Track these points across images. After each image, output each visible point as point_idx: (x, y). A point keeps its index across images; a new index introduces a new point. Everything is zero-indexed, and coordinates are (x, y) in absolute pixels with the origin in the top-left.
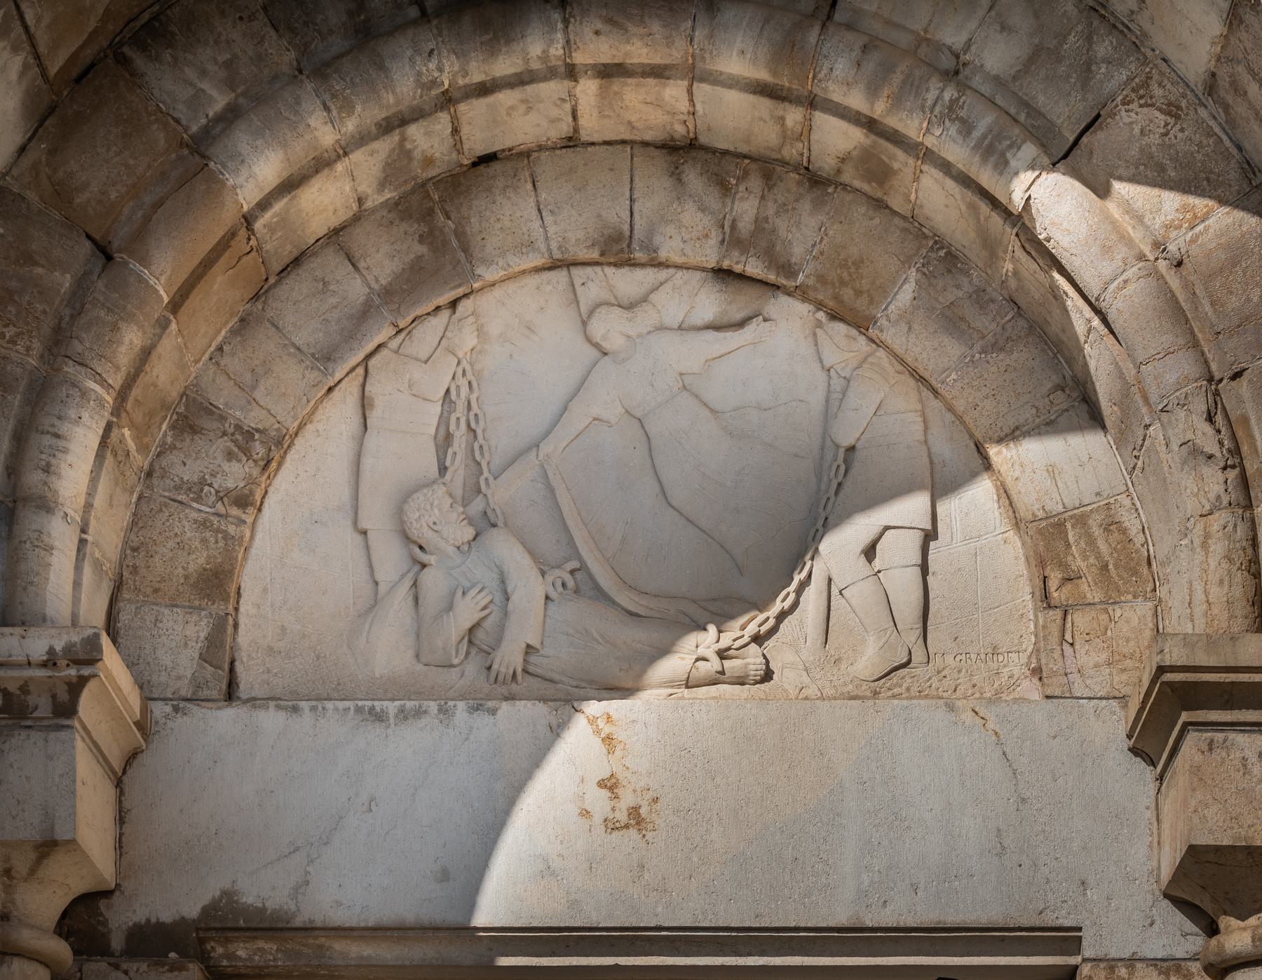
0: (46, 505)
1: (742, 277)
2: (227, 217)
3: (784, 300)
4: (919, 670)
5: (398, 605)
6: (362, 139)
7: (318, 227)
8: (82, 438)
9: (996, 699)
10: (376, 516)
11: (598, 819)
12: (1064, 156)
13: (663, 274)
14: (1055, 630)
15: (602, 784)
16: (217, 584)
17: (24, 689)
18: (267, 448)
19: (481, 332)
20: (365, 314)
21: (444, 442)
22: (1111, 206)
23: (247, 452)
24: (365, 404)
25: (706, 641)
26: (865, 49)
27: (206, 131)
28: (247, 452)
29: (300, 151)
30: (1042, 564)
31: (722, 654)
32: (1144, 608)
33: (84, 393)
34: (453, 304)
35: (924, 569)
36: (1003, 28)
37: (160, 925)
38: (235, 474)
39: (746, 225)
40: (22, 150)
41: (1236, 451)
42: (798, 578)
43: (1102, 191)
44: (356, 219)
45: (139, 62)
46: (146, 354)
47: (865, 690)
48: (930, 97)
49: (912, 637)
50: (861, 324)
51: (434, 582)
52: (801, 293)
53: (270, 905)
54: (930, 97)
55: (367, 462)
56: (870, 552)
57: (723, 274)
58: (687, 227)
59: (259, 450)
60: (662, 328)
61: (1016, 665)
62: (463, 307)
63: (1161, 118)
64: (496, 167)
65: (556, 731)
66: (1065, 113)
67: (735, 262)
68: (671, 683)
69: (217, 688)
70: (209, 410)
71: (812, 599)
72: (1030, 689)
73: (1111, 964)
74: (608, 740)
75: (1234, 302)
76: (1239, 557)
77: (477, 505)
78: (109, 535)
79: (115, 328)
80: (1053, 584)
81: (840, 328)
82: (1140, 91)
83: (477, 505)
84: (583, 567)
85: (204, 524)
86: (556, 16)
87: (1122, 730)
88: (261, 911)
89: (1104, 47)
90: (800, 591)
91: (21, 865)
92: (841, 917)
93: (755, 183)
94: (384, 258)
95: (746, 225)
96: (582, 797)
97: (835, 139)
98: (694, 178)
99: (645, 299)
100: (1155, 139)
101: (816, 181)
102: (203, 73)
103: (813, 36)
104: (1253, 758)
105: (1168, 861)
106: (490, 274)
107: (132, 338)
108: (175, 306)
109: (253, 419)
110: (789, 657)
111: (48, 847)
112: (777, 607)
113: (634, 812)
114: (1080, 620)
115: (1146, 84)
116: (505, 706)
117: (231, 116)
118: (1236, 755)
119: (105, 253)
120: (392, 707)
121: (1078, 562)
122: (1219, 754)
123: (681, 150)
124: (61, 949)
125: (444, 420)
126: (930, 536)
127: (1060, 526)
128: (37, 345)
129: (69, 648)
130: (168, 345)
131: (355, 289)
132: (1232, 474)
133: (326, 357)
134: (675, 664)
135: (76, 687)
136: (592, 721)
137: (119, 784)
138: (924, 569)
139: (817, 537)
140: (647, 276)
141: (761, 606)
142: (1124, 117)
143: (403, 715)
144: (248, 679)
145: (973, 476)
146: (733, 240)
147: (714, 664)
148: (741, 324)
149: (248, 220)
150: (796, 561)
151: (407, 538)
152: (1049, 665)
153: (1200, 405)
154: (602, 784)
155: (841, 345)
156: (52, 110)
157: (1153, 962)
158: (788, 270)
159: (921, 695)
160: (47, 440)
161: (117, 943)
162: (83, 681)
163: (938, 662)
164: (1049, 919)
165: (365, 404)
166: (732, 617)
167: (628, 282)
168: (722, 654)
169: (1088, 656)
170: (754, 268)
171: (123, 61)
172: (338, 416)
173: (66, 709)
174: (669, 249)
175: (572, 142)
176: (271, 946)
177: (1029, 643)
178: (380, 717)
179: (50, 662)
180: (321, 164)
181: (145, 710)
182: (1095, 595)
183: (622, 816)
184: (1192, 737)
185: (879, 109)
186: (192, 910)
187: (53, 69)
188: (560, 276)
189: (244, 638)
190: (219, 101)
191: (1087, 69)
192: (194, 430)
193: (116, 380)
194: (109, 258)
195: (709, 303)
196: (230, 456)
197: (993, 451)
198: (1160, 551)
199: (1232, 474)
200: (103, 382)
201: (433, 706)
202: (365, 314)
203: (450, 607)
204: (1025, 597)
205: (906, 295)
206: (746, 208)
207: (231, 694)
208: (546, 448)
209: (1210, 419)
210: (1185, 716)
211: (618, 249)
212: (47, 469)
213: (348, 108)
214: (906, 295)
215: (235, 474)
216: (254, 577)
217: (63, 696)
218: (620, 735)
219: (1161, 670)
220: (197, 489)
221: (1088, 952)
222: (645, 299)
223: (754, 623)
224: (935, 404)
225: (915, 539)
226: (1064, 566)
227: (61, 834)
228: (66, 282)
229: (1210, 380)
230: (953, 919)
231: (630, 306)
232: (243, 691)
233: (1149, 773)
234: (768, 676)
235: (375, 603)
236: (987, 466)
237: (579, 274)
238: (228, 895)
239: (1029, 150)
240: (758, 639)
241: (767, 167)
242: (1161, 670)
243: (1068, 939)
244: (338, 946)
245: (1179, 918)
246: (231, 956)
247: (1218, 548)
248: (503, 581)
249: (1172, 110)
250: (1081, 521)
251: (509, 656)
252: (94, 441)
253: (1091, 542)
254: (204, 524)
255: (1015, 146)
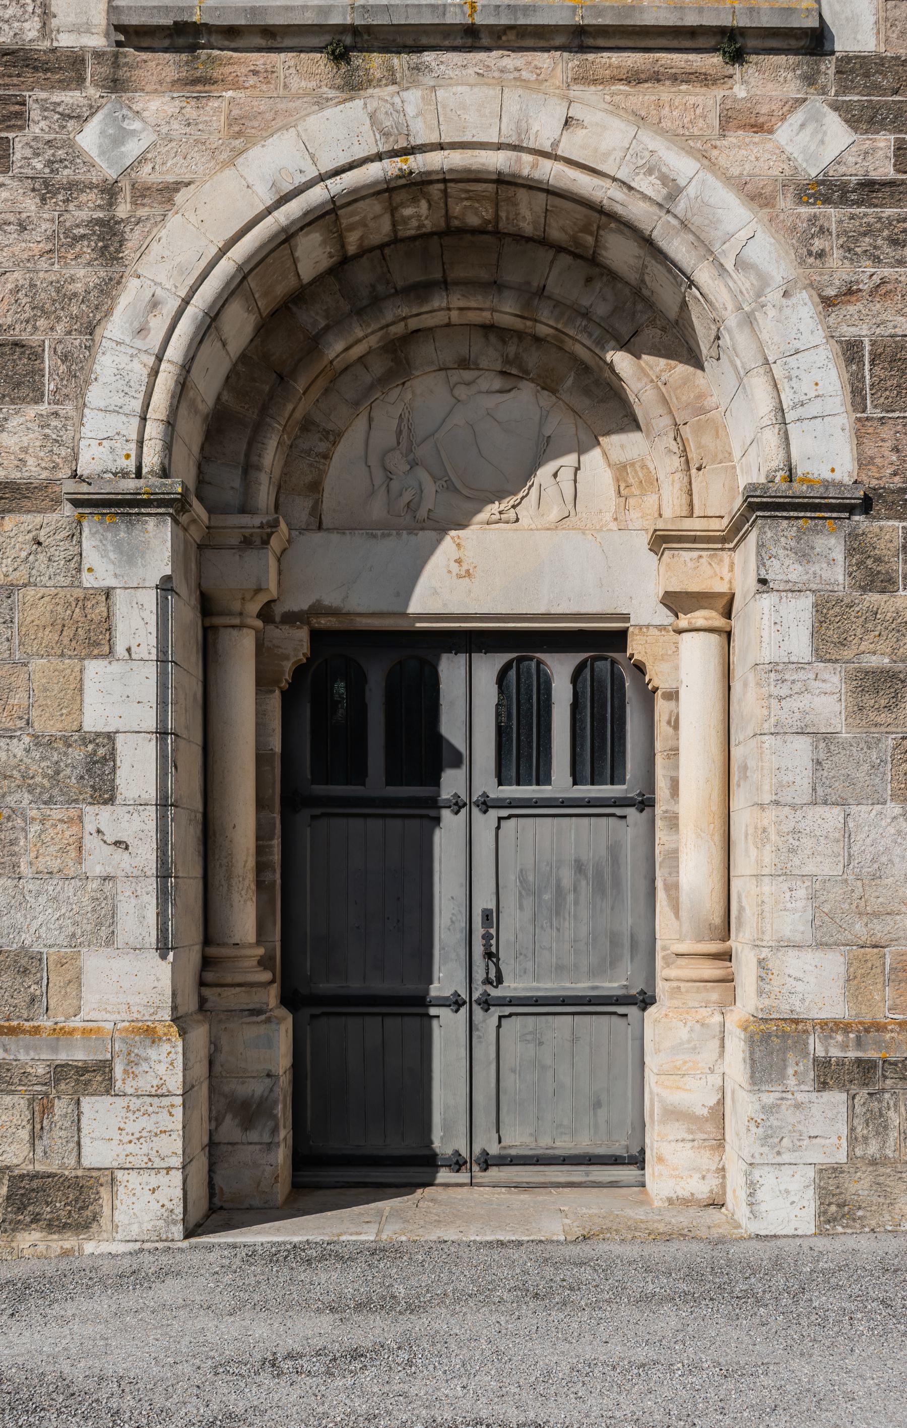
0: (259, 468)
1: (510, 374)
2: (325, 362)
3: (525, 382)
4: (573, 518)
5: (382, 494)
6: (373, 333)
7: (355, 357)
8: (272, 444)
9: (600, 530)
10: (374, 461)
11: (454, 574)
12: (624, 345)
13: (481, 372)
14: (622, 504)
15: (456, 561)
16: (315, 487)
17: (251, 535)
18: (334, 437)
19: (413, 393)
20: (372, 387)
21: (399, 433)
22: (642, 362)
23: (327, 439)
24: (370, 420)
25: (495, 507)
26: (554, 307)
27: (318, 333)
28: (327, 439)
29: (351, 340)
30: (618, 481)
31: (500, 513)
32: (655, 497)
33: (273, 428)
34: (404, 384)
35: (575, 481)
36: (604, 299)
37: (293, 612)
38: (322, 447)
39: (511, 356)
40: (252, 340)
41: (685, 450)
42: (529, 484)
43: (638, 357)
44: (368, 353)
45: (294, 309)
46: (294, 409)
47: (553, 526)
48: (578, 324)
49: (570, 506)
50: (554, 391)
51: (395, 486)
52: (532, 380)
53: (334, 605)
54: (578, 324)
55: (371, 441)
56: (555, 475)
57: (503, 373)
58: (490, 356)
59: (331, 438)
60: (480, 392)
61: (608, 517)
62: (408, 384)
63: (659, 332)
64: (420, 333)
65: (439, 541)
66: (625, 330)
67: (507, 369)
68: (481, 523)
69: (315, 526)
70: (313, 423)
71: (534, 491)
72: (613, 526)
73: (640, 627)
74: (458, 545)
75: (684, 398)
76: (685, 489)
77: (411, 457)
78: (277, 473)
79: (285, 405)
80: (622, 488)
81: (546, 392)
82: (652, 322)
83: (411, 457)
84: (450, 479)
85: (311, 465)
86: (444, 294)
87: (646, 541)
88: (330, 607)
89: (639, 307)
90: (529, 489)
91: (248, 597)
92: (542, 610)
93: (515, 340)
94: (378, 367)
95: (511, 356)
96: (448, 566)
97: (543, 330)
98: (493, 339)
99: (474, 381)
100: (657, 340)
101: (538, 340)
102: (317, 314)
103: (536, 302)
104: (688, 560)
105: (661, 594)
106: (417, 373)
107: (290, 407)
108: (304, 393)
109: (330, 426)
110: (525, 513)
111: (258, 590)
112: (521, 495)
113: (468, 571)
114: (632, 501)
115: (654, 320)
116: (421, 533)
117: (327, 328)
118: (682, 559)
119: (281, 377)
120: (379, 533)
121: (631, 480)
122: (676, 559)
123: (488, 329)
124: (259, 624)
125: (399, 425)
126: (577, 469)
127: (625, 466)
128: (256, 411)
129: (268, 522)
130: (301, 405)
131: (368, 379)
132: (683, 459)
133: (356, 404)
134: (483, 516)
135: (269, 535)
136: (452, 538)
137: (279, 560)
138: (575, 481)
139: (536, 469)
140: (476, 373)
141: (515, 494)
142: (646, 331)
143: (383, 536)
144: (326, 523)
145: (594, 447)
146: (507, 361)
147: (498, 516)
148: (509, 391)
149: (331, 362)
150: (528, 478)
151: (385, 469)
152: (620, 518)
153: (672, 435)
154: (456, 561)
155: (546, 399)
156: (262, 326)
157: (656, 626)
158: (527, 373)
159: (574, 529)
160: (260, 445)
161: (278, 619)
162: (272, 533)
163: (579, 515)
164: (618, 611)
165: (370, 420)
166: (504, 498)
167: (468, 375)
168: (500, 513)
169: (634, 514)
170: (514, 371)
171: (289, 309)
172: (361, 424)
173: (266, 542)
174: (483, 363)
175: (448, 325)
176: (333, 619)
177: (613, 509)
178: (374, 536)
179: (262, 526)
180: (358, 341)
181: (290, 534)
182: (636, 492)
183: (463, 573)
184: (667, 553)
185: (559, 326)
186: (305, 607)
187: (264, 315)
188: (443, 373)
189: (325, 506)
190: (323, 323)
191: (633, 315)
192: (308, 430)
193: (283, 423)
194: (282, 378)
195: (497, 383)
196: (321, 440)
197: (601, 439)
198: (661, 477)
199: (683, 459)
200: (280, 424)
201: (394, 532)
202: (372, 387)
203: (401, 495)
204: (612, 492)
205: (570, 382)
206: (512, 349)
207: (320, 528)
208: (436, 436)
209: (675, 439)
210: (664, 546)
211: (464, 364)
212: (260, 456)
213: (369, 325)
214: (570, 382)
215: (322, 447)
216: (328, 484)
217: (265, 538)
218: (463, 543)
219: (656, 530)
220: (309, 452)
221: (632, 623)
222: (474, 381)
223: (513, 500)
224: (579, 420)
225: (572, 470)
226: (626, 481)
227: (264, 586)
228: (267, 388)
229: (676, 425)
230: (583, 611)
231: (468, 384)
232: (324, 526)
233: (656, 558)
234: (517, 520)
235: (373, 492)
236: (599, 444)
237: (450, 372)
238: (319, 601)
239: (613, 343)
240: (514, 507)
241: (520, 335)
242: (656, 530)
243: (626, 618)
244: (358, 619)
245: (665, 610)
246: (319, 623)
247: (677, 486)
248: (420, 485)
249: (664, 329)
250: (633, 465)
251: (422, 513)
252: (275, 444)
253: (636, 472)
254: (311, 465)
255: (607, 342)
